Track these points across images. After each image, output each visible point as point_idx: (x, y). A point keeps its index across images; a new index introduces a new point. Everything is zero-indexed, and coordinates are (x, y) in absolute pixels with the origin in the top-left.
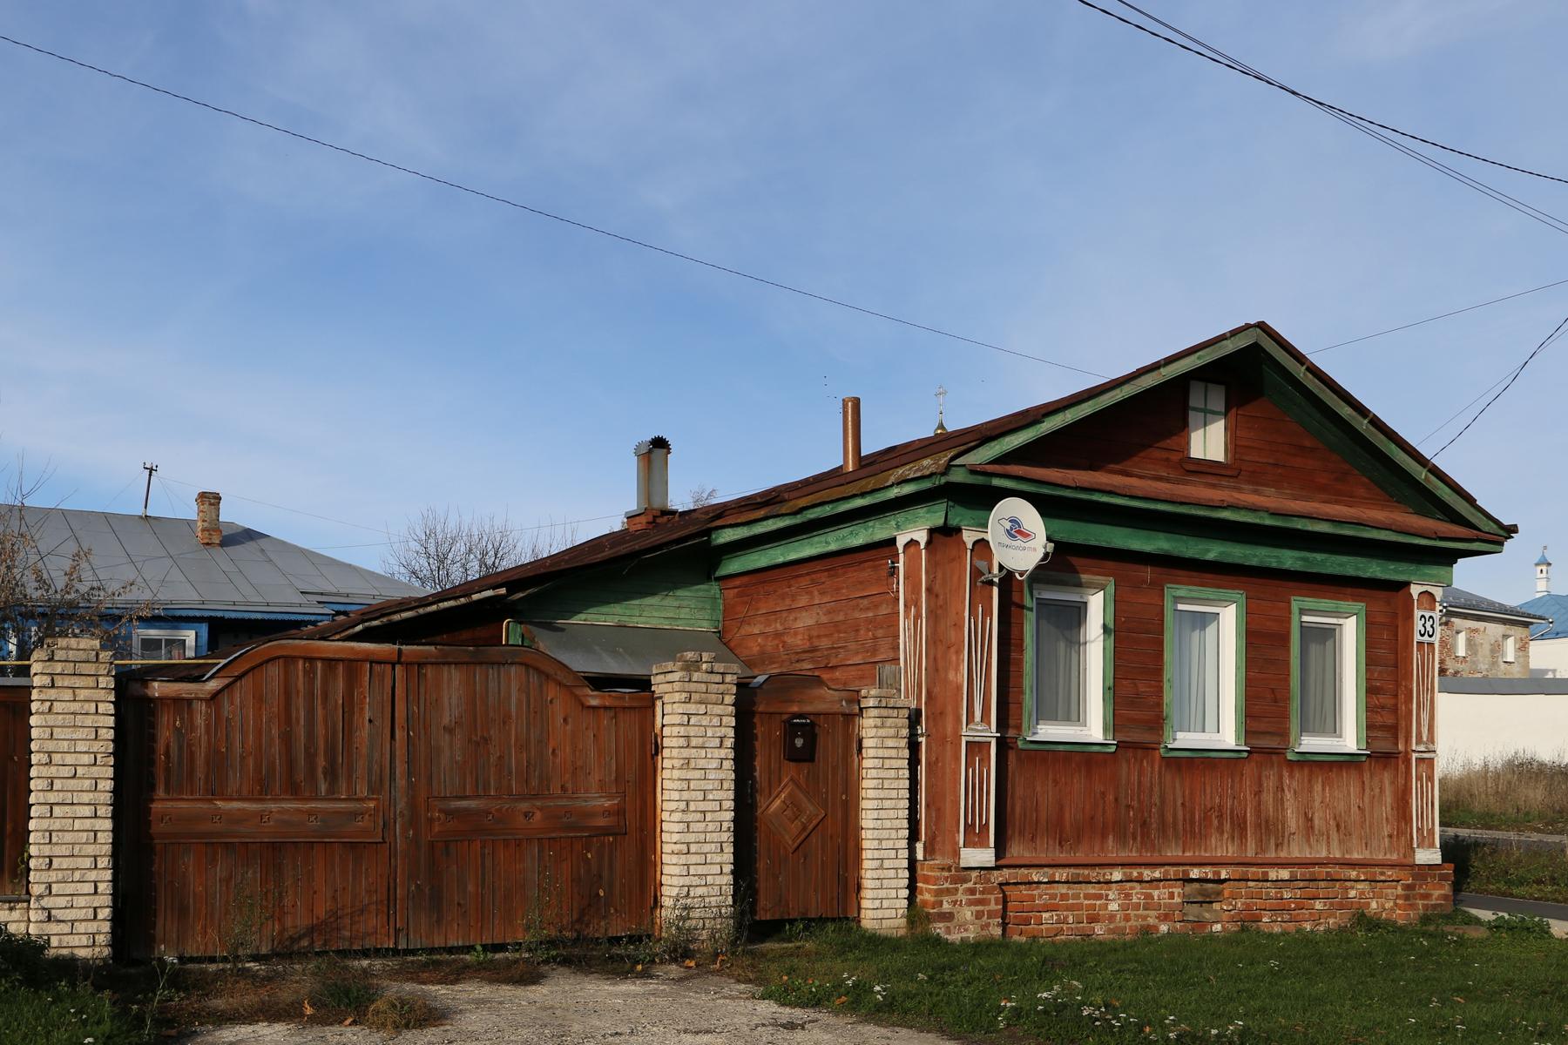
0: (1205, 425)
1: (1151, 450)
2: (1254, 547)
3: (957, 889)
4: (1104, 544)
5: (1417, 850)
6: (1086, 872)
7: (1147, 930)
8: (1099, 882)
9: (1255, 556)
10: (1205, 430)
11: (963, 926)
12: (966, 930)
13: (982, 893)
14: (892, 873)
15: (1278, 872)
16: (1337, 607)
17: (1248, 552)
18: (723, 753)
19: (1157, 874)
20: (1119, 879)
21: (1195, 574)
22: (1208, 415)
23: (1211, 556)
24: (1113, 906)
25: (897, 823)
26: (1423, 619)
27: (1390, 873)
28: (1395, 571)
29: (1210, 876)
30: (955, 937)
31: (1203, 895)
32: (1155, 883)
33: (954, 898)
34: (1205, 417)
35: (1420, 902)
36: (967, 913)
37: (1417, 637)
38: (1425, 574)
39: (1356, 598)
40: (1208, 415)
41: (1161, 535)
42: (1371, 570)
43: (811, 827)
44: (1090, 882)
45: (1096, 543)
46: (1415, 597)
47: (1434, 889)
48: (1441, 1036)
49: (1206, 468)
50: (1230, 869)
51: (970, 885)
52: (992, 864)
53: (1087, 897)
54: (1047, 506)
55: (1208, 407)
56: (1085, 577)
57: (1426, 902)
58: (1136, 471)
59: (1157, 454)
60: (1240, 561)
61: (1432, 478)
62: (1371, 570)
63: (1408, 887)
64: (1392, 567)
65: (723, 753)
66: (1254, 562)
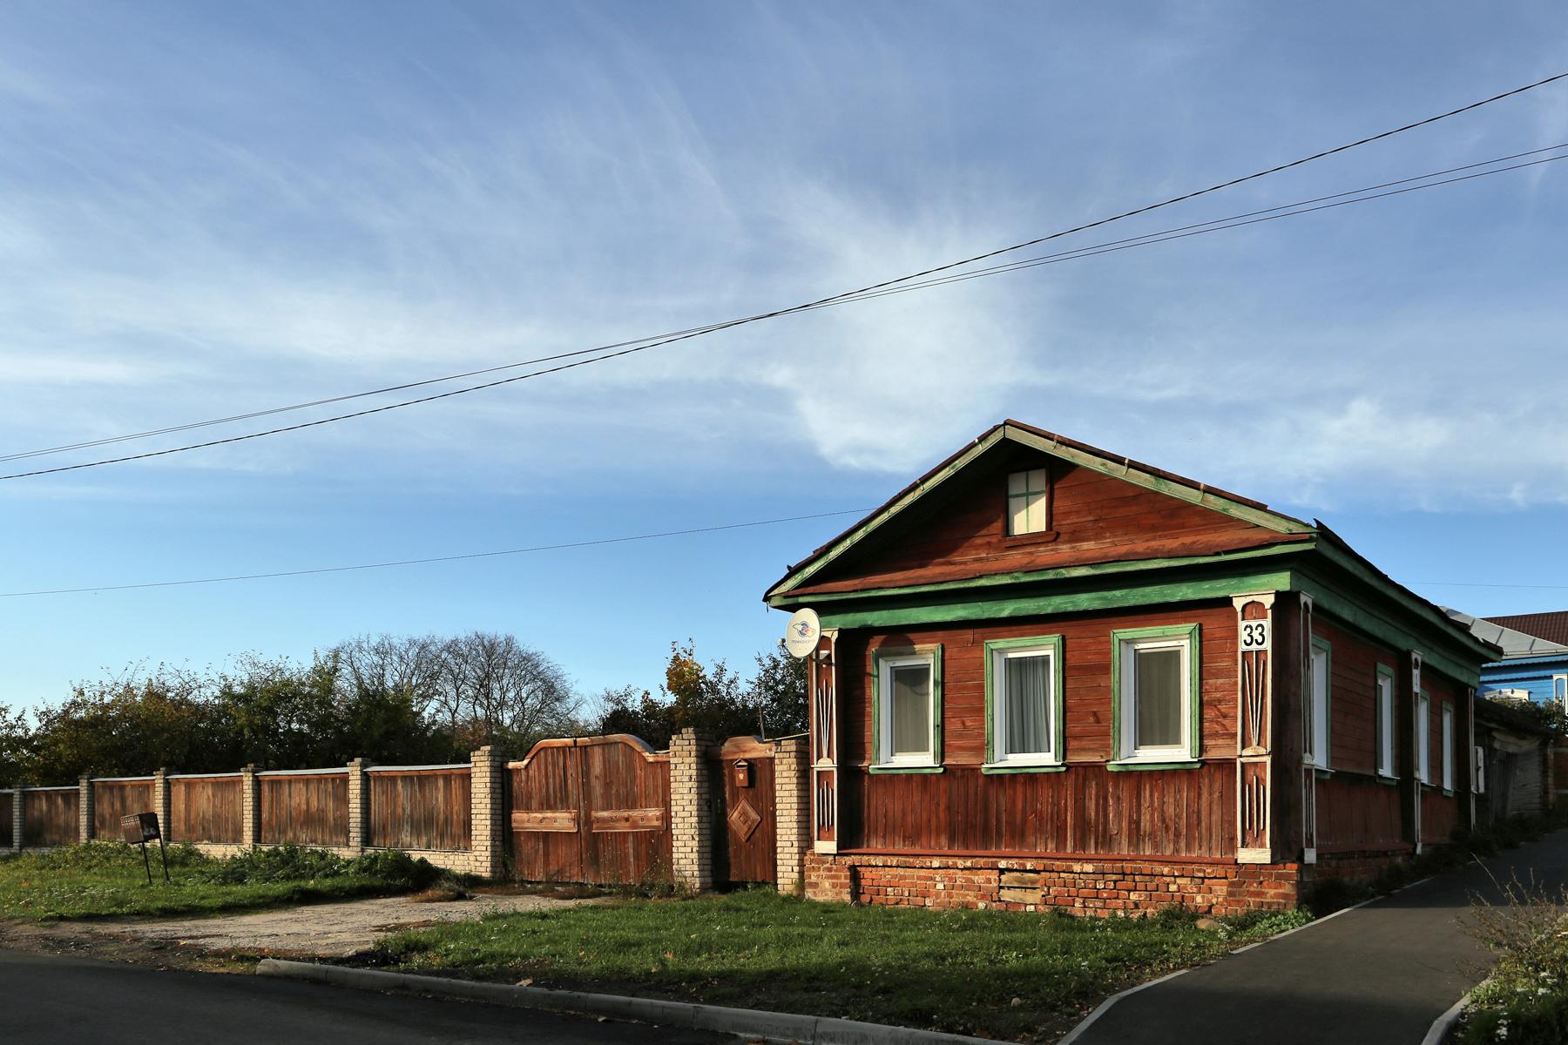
0: (1028, 506)
1: (973, 539)
2: (1048, 598)
3: (819, 868)
4: (913, 622)
5: (1306, 849)
6: (911, 860)
7: (966, 907)
8: (922, 868)
9: (1049, 605)
10: (1028, 512)
11: (824, 891)
12: (826, 895)
13: (836, 871)
14: (788, 856)
15: (1081, 865)
16: (1163, 633)
17: (1041, 604)
18: (690, 784)
19: (969, 864)
20: (937, 866)
21: (1014, 628)
22: (1030, 497)
23: (1005, 614)
24: (940, 886)
25: (790, 825)
26: (1249, 629)
27: (1209, 871)
28: (1211, 589)
29: (1016, 867)
30: (820, 898)
31: (1020, 882)
32: (974, 871)
33: (818, 873)
34: (1027, 499)
35: (1251, 900)
36: (827, 884)
37: (1242, 647)
38: (1255, 585)
39: (1186, 620)
40: (1029, 497)
41: (959, 606)
42: (1181, 594)
43: (754, 827)
44: (915, 867)
45: (907, 623)
46: (1239, 609)
47: (1271, 888)
48: (259, 867)
49: (1032, 540)
50: (1034, 862)
51: (828, 865)
52: (835, 852)
53: (919, 878)
54: (822, 609)
55: (1030, 490)
56: (917, 647)
57: (1258, 900)
58: (958, 559)
59: (979, 541)
60: (1035, 613)
61: (1211, 498)
62: (1181, 594)
63: (1232, 884)
64: (1207, 586)
65: (690, 784)
66: (1049, 610)
